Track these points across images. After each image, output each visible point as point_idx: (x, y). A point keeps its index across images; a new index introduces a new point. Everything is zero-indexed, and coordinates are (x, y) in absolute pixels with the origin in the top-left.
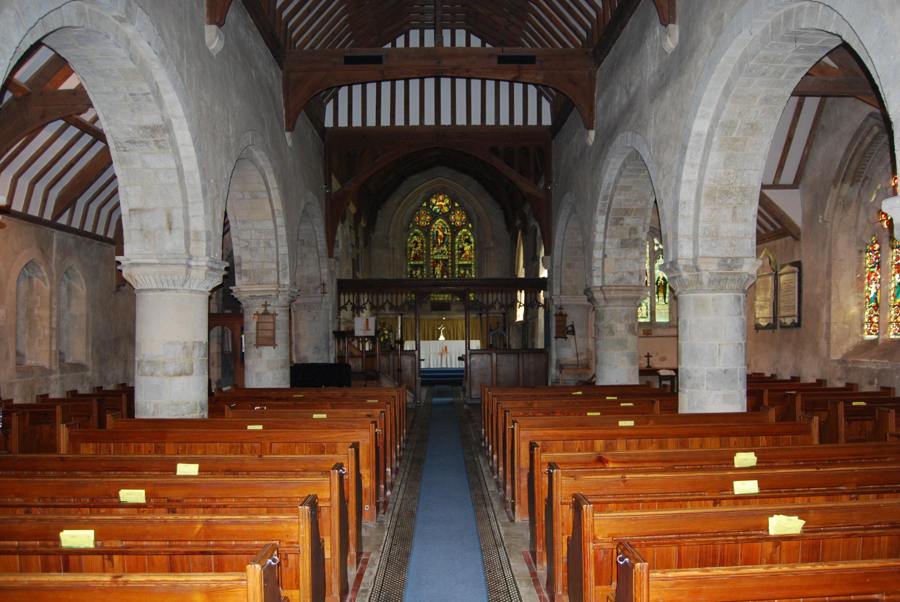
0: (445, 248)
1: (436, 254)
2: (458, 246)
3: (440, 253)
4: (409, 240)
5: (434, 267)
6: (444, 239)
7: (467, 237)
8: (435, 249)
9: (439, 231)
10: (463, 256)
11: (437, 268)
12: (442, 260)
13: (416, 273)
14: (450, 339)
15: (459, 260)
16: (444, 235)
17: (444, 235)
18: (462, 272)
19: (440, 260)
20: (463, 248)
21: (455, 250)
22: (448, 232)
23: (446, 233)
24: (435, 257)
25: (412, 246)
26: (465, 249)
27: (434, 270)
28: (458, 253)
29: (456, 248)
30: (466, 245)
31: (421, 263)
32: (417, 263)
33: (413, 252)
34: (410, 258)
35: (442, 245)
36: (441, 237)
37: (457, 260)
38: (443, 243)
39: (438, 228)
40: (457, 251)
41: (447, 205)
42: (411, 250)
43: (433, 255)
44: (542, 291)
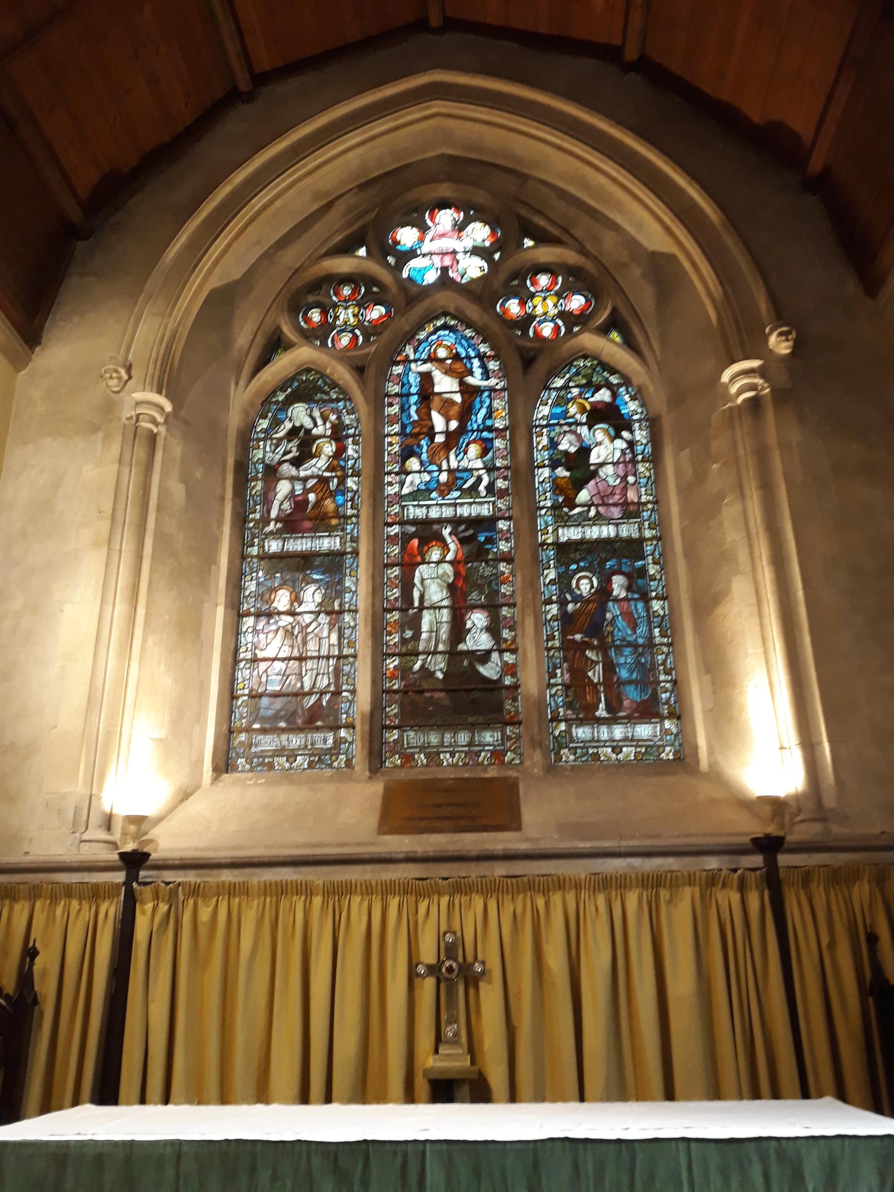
3: (444, 489)
6: (466, 413)
15: (563, 521)
37: (545, 519)
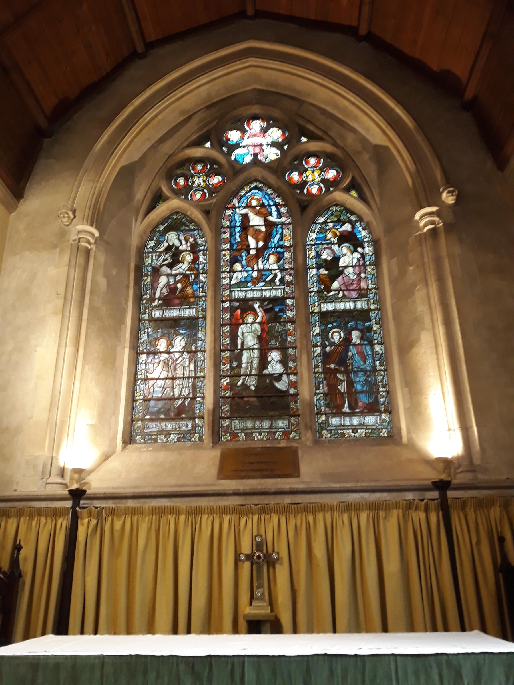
0: (271, 263)
1: (240, 284)
2: (318, 255)
3: (255, 281)
4: (152, 244)
5: (235, 325)
6: (268, 237)
7: (347, 227)
8: (238, 266)
9: (252, 216)
10: (335, 285)
11: (243, 328)
12: (262, 300)
13: (171, 344)
14: (115, 633)
15: (324, 299)
16: (270, 225)
17: (270, 225)
18: (336, 337)
19: (253, 299)
20: (336, 259)
21: (306, 268)
22: (280, 215)
23: (273, 218)
24: (239, 294)
25: (157, 263)
26: (341, 264)
27: (234, 336)
28: (319, 276)
29: (312, 262)
30: (345, 249)
31: (188, 312)
32: (172, 313)
33: (163, 280)
34: (153, 299)
35: (260, 253)
36: (256, 233)
37: (313, 298)
38: (266, 247)
39: (248, 206)
40: (314, 271)
41: (274, 144)
42: (156, 272)
43: (230, 286)
44: (326, 272)
